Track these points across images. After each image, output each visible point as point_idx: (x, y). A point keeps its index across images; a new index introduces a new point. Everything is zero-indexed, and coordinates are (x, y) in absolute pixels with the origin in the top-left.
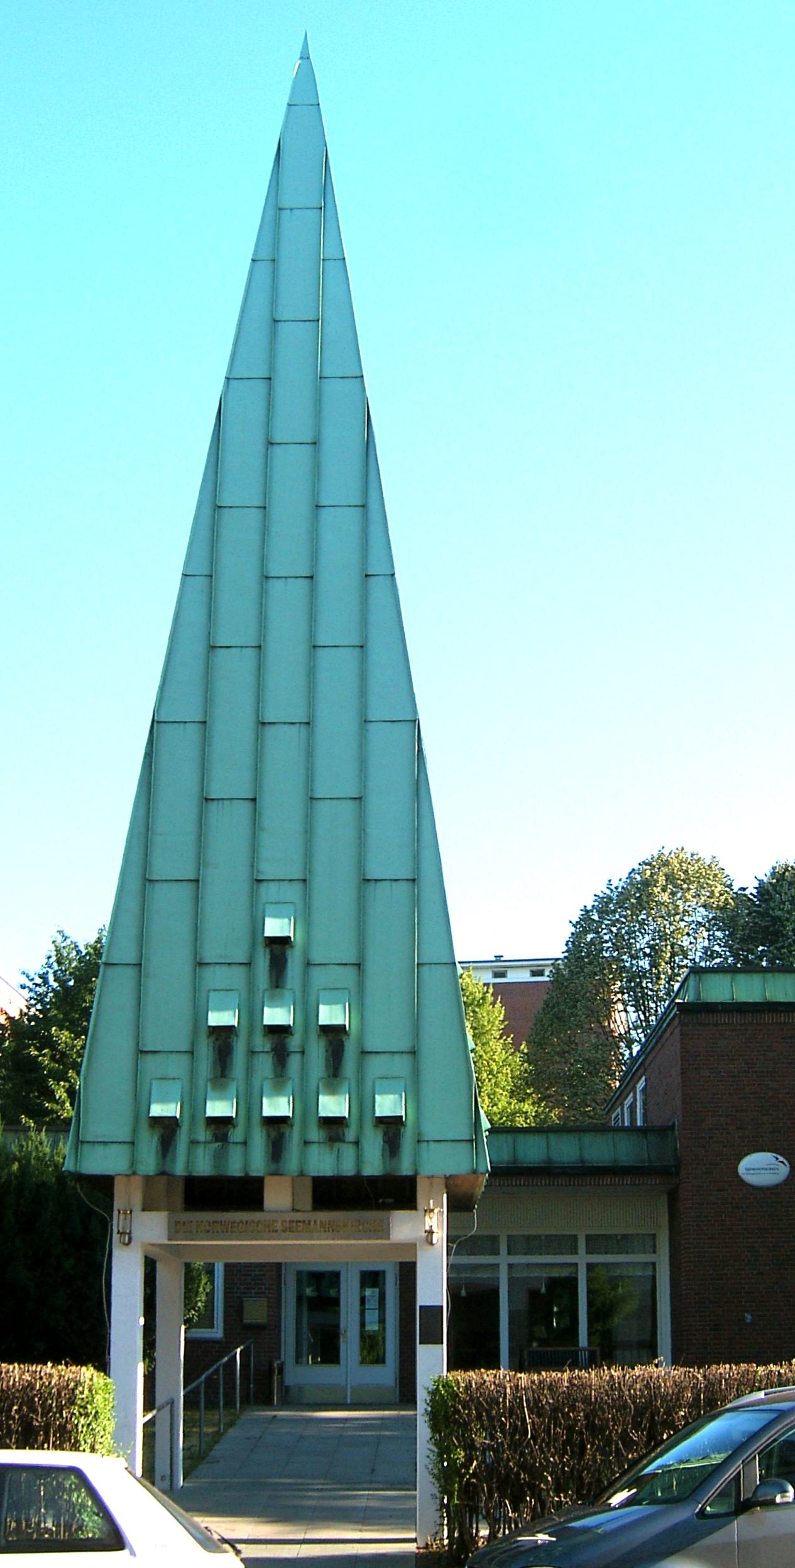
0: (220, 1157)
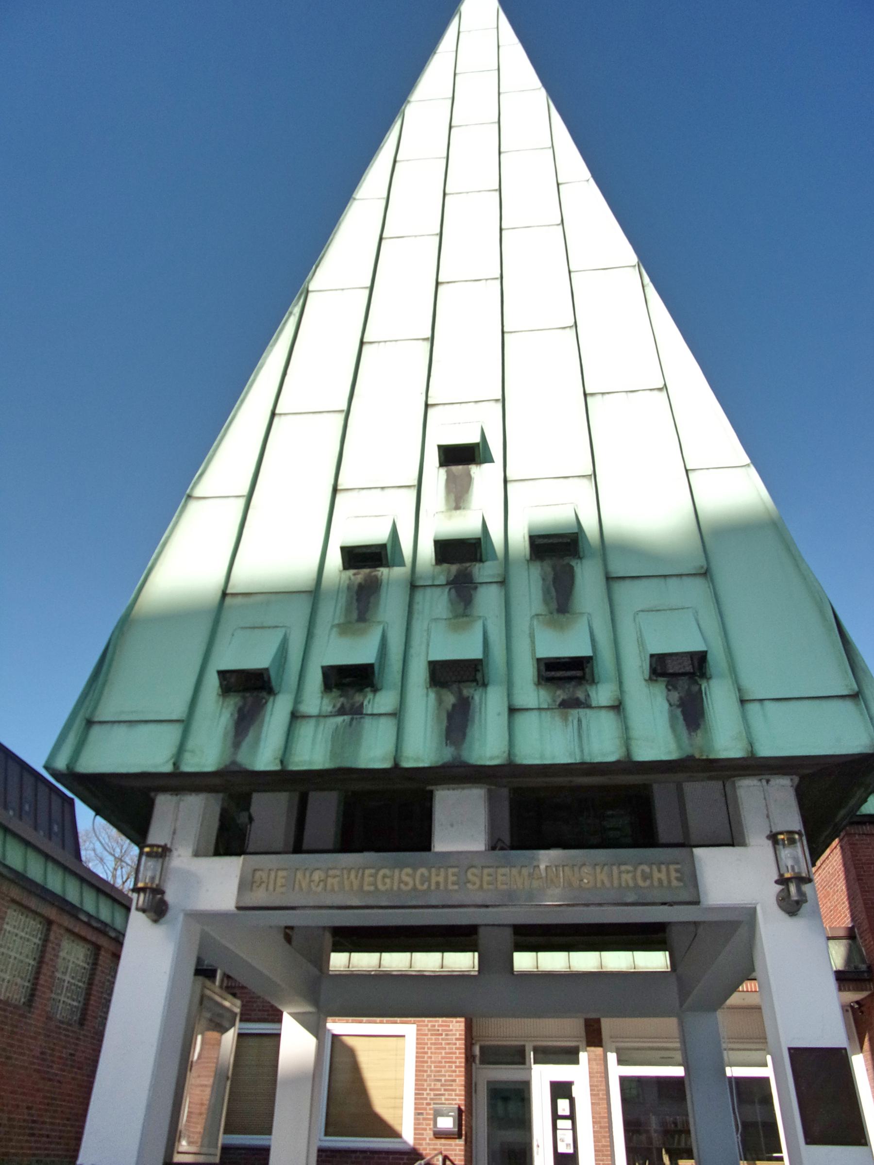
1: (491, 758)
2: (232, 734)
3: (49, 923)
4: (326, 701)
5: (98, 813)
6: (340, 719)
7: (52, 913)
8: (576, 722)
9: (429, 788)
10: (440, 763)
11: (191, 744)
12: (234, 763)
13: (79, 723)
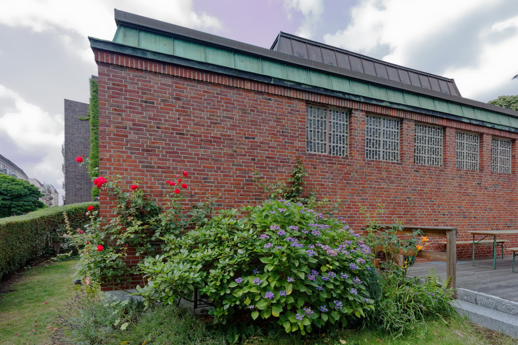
3: (444, 128)
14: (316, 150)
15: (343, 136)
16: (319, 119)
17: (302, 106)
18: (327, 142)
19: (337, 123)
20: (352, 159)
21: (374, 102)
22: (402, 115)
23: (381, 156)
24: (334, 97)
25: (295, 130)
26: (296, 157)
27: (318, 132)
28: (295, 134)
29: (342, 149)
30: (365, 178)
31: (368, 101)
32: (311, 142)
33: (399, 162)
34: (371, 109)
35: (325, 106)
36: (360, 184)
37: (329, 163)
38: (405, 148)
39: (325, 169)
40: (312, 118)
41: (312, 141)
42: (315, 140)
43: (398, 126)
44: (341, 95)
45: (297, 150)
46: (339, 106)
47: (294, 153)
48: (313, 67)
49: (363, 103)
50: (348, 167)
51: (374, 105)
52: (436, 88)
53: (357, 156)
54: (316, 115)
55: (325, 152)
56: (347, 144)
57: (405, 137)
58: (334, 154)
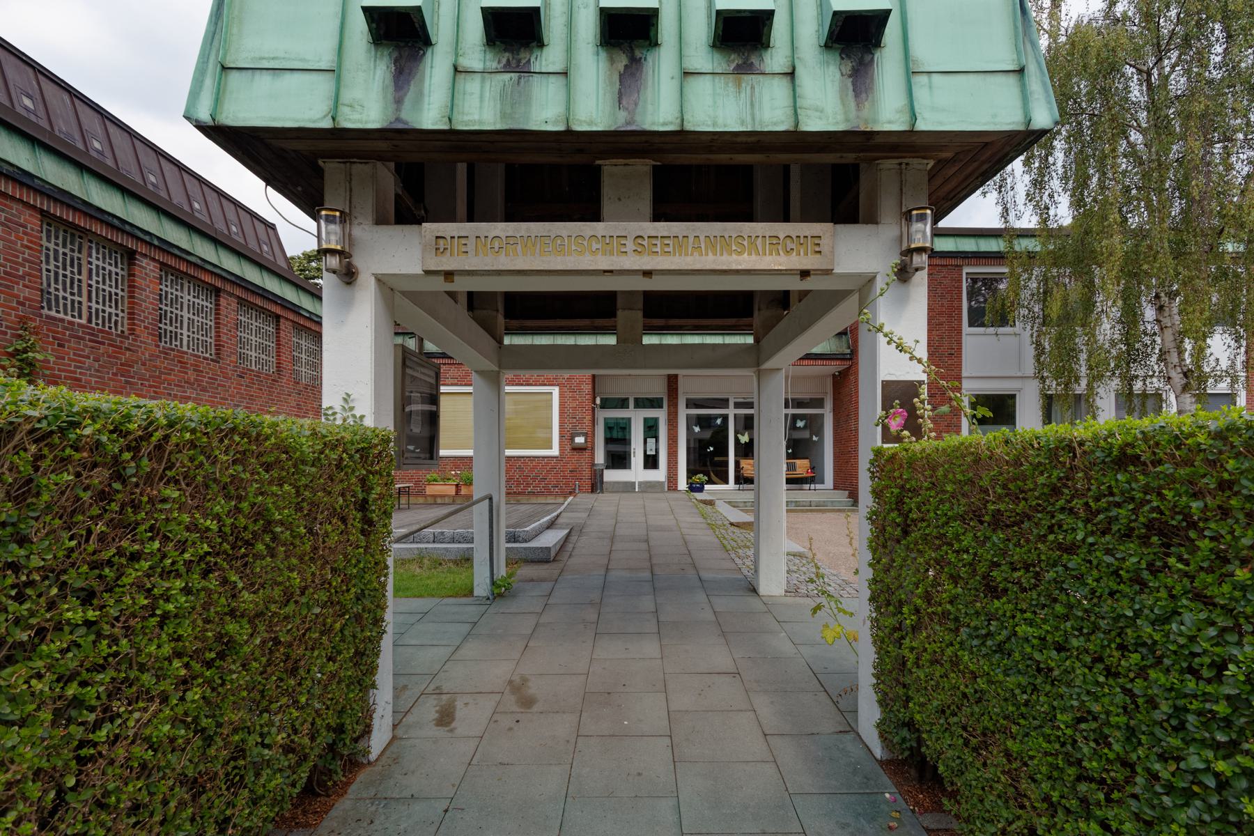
0: (514, 99)
1: (664, 124)
2: (391, 89)
3: (278, 317)
4: (489, 56)
5: (268, 183)
6: (507, 76)
7: (278, 311)
8: (749, 88)
9: (598, 162)
10: (612, 129)
11: (346, 96)
12: (398, 120)
13: (212, 68)
14: (61, 309)
15: (116, 294)
16: (67, 251)
17: (32, 221)
18: (84, 299)
19: (104, 269)
20: (135, 340)
21: (176, 252)
22: (219, 284)
23: (185, 343)
24: (102, 221)
25: (17, 263)
26: (16, 316)
27: (65, 276)
28: (18, 270)
29: (114, 318)
30: (159, 377)
31: (165, 247)
32: (49, 293)
33: (214, 357)
34: (171, 262)
35: (84, 232)
36: (151, 386)
37: (90, 341)
38: (224, 338)
39: (83, 350)
40: (52, 246)
41: (52, 290)
42: (57, 289)
43: (57, 238)
44: (116, 222)
45: (23, 304)
46: (111, 240)
47: (13, 309)
48: (47, 141)
49: (155, 247)
50: (128, 353)
51: (176, 256)
52: (178, 198)
53: (144, 336)
54: (60, 241)
55: (80, 317)
56: (123, 311)
57: (223, 320)
58: (97, 324)
